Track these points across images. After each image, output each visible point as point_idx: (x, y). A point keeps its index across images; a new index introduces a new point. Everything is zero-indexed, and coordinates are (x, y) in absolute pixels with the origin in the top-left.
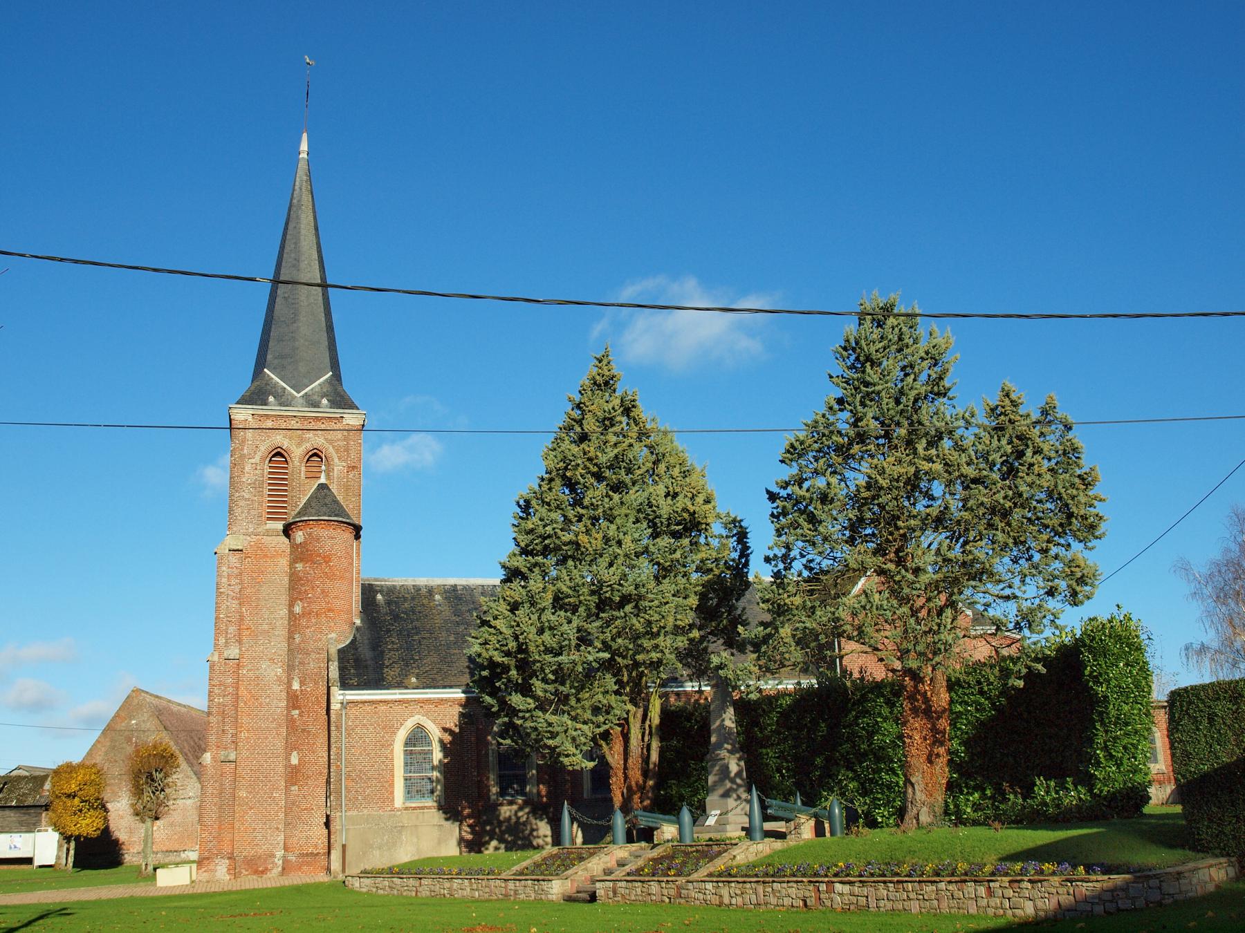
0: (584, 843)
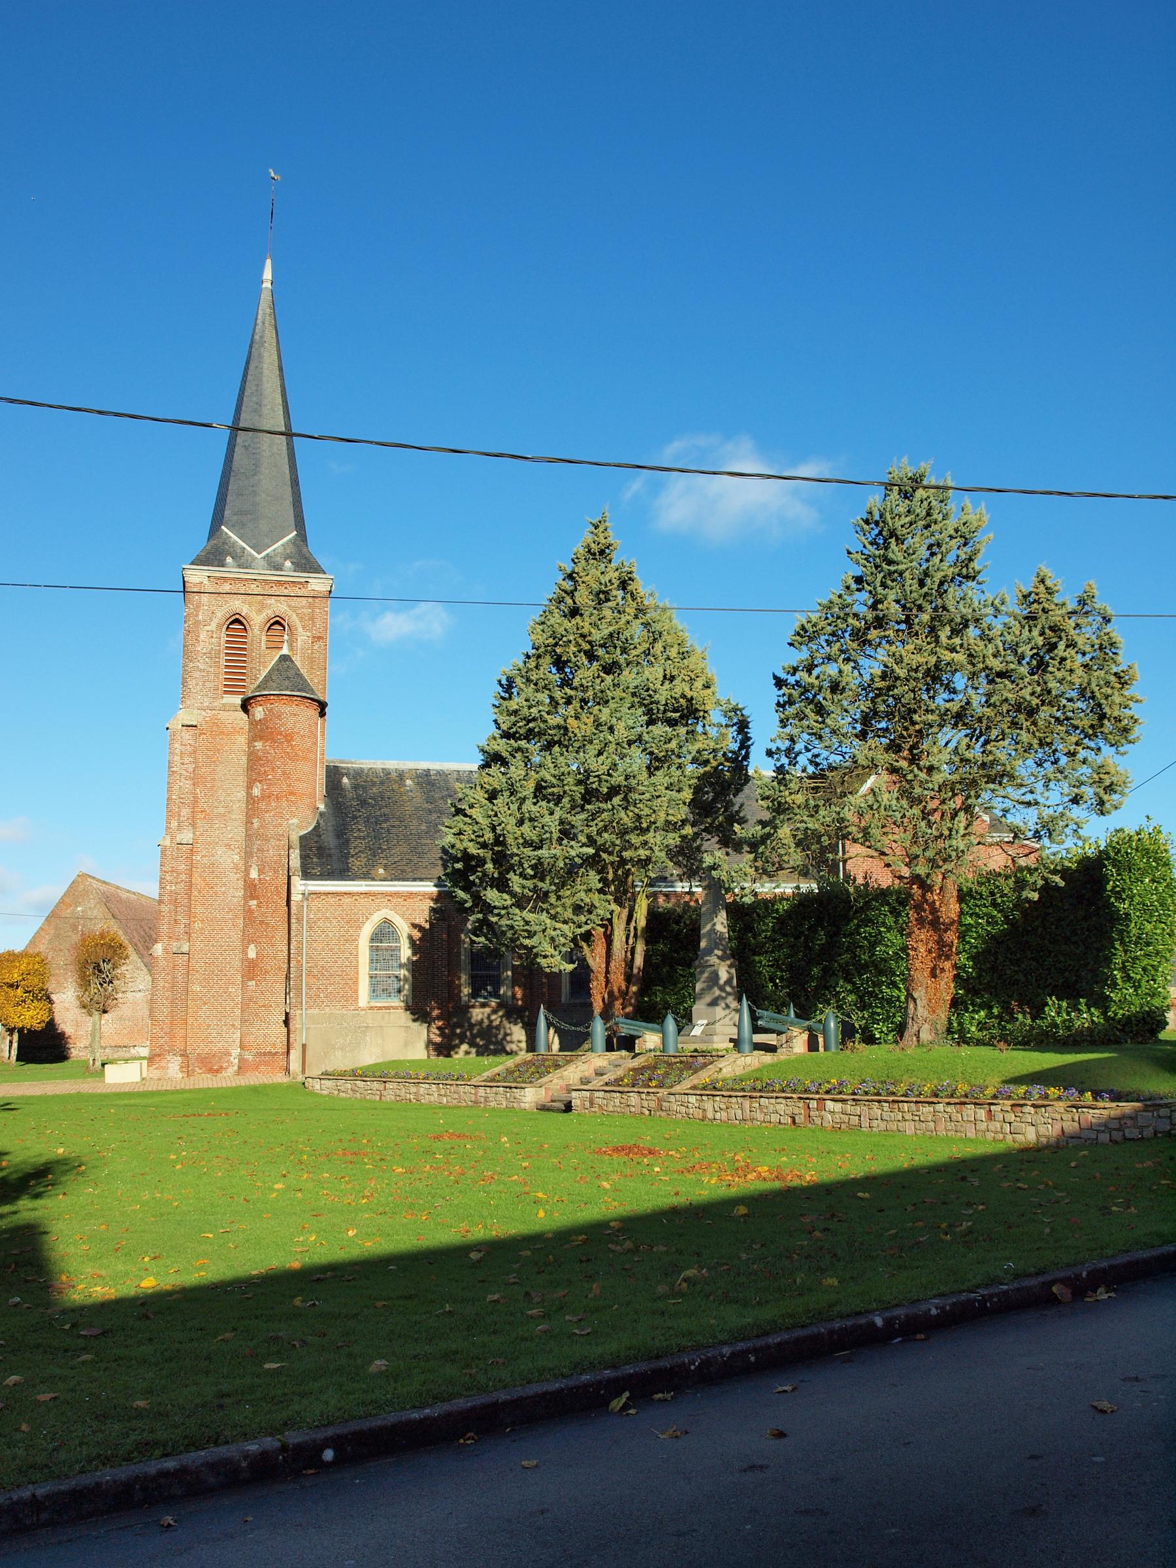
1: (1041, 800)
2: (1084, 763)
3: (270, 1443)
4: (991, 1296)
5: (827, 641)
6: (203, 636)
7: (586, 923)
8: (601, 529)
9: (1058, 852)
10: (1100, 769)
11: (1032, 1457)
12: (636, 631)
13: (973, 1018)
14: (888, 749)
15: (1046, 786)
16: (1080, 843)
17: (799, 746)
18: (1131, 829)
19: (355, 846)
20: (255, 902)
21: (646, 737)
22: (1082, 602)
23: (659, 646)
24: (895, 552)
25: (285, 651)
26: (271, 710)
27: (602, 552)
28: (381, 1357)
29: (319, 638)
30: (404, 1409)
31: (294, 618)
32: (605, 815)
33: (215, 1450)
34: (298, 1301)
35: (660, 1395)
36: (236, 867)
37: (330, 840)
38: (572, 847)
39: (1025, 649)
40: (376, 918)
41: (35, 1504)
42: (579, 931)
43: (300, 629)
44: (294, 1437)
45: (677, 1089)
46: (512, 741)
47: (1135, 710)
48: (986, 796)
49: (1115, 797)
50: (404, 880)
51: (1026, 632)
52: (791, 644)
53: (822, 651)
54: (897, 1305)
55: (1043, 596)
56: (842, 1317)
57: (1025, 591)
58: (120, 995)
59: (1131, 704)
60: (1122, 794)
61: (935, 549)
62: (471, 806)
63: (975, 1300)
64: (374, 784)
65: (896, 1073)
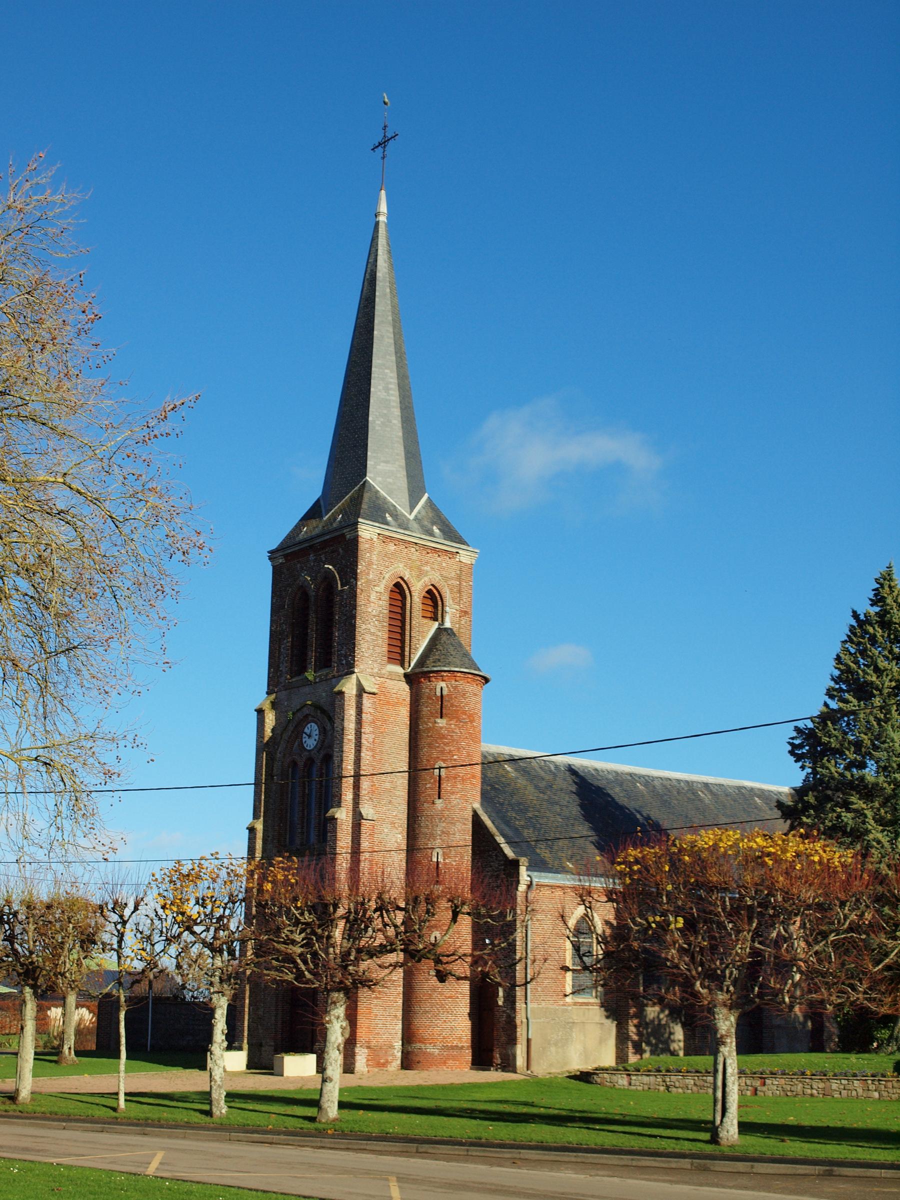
0: (685, 1055)
26: (455, 688)
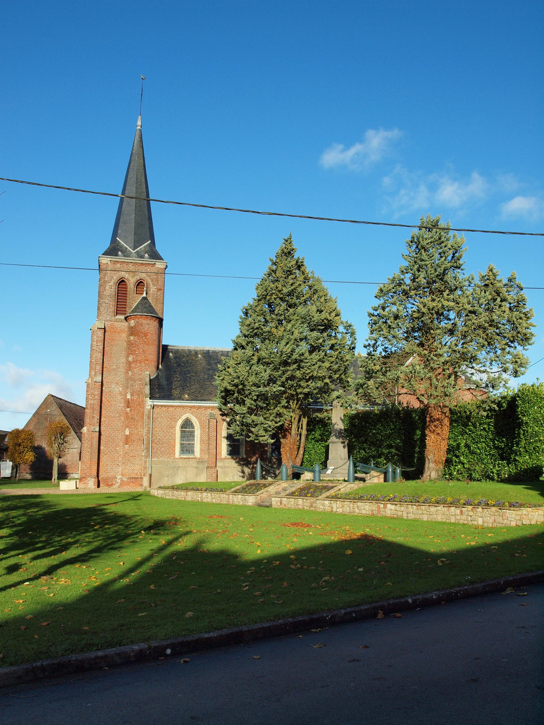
1: (488, 370)
2: (508, 353)
3: (143, 646)
4: (460, 591)
5: (392, 296)
6: (107, 288)
7: (280, 421)
8: (289, 242)
9: (496, 394)
10: (516, 356)
11: (476, 659)
12: (304, 289)
13: (455, 469)
14: (418, 345)
15: (491, 364)
16: (506, 390)
17: (379, 343)
18: (530, 384)
19: (175, 384)
20: (129, 409)
21: (308, 337)
22: (510, 280)
23: (316, 296)
24: (424, 256)
25: (144, 295)
27: (289, 253)
28: (191, 611)
29: (160, 289)
30: (201, 632)
31: (149, 280)
32: (289, 373)
33: (120, 648)
34: (152, 587)
35: (313, 630)
36: (121, 393)
37: (164, 382)
38: (274, 387)
39: (482, 301)
40: (184, 417)
41: (43, 668)
42: (276, 425)
43: (151, 285)
44: (154, 644)
45: (320, 497)
46: (247, 338)
47: (532, 330)
48: (464, 367)
49: (522, 369)
50: (197, 400)
51: (483, 292)
52: (376, 297)
53: (390, 300)
54: (418, 594)
55: (492, 277)
56: (393, 598)
57: (484, 274)
58: (67, 450)
59: (531, 327)
60: (526, 368)
61: (442, 255)
62: (229, 368)
63: (453, 592)
64: (184, 356)
65: (419, 493)
